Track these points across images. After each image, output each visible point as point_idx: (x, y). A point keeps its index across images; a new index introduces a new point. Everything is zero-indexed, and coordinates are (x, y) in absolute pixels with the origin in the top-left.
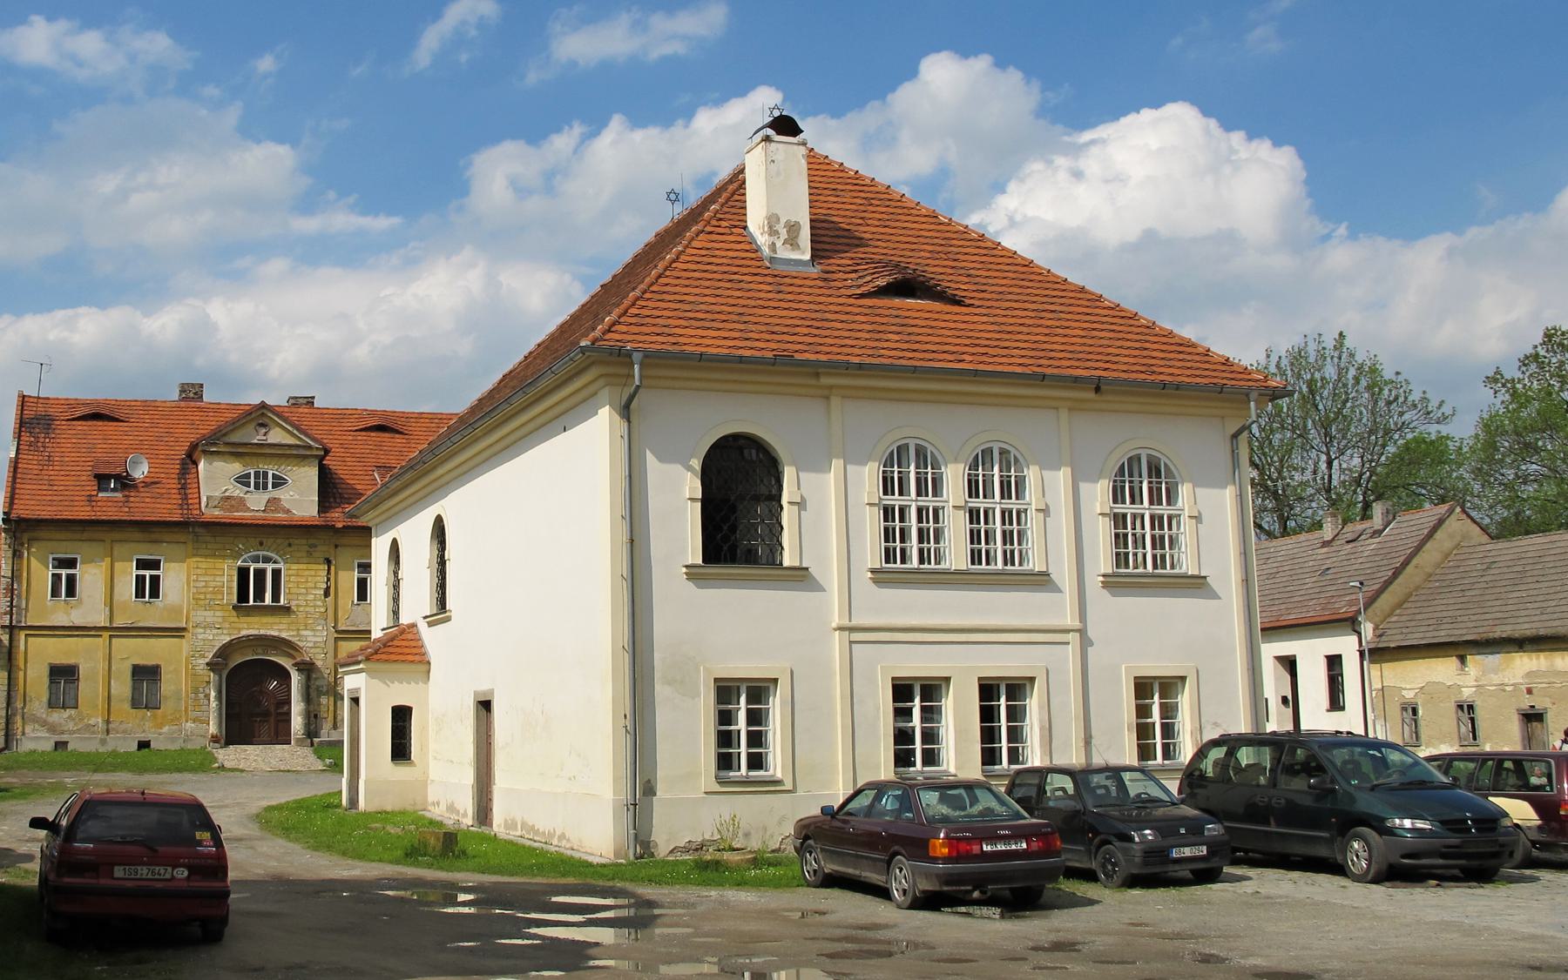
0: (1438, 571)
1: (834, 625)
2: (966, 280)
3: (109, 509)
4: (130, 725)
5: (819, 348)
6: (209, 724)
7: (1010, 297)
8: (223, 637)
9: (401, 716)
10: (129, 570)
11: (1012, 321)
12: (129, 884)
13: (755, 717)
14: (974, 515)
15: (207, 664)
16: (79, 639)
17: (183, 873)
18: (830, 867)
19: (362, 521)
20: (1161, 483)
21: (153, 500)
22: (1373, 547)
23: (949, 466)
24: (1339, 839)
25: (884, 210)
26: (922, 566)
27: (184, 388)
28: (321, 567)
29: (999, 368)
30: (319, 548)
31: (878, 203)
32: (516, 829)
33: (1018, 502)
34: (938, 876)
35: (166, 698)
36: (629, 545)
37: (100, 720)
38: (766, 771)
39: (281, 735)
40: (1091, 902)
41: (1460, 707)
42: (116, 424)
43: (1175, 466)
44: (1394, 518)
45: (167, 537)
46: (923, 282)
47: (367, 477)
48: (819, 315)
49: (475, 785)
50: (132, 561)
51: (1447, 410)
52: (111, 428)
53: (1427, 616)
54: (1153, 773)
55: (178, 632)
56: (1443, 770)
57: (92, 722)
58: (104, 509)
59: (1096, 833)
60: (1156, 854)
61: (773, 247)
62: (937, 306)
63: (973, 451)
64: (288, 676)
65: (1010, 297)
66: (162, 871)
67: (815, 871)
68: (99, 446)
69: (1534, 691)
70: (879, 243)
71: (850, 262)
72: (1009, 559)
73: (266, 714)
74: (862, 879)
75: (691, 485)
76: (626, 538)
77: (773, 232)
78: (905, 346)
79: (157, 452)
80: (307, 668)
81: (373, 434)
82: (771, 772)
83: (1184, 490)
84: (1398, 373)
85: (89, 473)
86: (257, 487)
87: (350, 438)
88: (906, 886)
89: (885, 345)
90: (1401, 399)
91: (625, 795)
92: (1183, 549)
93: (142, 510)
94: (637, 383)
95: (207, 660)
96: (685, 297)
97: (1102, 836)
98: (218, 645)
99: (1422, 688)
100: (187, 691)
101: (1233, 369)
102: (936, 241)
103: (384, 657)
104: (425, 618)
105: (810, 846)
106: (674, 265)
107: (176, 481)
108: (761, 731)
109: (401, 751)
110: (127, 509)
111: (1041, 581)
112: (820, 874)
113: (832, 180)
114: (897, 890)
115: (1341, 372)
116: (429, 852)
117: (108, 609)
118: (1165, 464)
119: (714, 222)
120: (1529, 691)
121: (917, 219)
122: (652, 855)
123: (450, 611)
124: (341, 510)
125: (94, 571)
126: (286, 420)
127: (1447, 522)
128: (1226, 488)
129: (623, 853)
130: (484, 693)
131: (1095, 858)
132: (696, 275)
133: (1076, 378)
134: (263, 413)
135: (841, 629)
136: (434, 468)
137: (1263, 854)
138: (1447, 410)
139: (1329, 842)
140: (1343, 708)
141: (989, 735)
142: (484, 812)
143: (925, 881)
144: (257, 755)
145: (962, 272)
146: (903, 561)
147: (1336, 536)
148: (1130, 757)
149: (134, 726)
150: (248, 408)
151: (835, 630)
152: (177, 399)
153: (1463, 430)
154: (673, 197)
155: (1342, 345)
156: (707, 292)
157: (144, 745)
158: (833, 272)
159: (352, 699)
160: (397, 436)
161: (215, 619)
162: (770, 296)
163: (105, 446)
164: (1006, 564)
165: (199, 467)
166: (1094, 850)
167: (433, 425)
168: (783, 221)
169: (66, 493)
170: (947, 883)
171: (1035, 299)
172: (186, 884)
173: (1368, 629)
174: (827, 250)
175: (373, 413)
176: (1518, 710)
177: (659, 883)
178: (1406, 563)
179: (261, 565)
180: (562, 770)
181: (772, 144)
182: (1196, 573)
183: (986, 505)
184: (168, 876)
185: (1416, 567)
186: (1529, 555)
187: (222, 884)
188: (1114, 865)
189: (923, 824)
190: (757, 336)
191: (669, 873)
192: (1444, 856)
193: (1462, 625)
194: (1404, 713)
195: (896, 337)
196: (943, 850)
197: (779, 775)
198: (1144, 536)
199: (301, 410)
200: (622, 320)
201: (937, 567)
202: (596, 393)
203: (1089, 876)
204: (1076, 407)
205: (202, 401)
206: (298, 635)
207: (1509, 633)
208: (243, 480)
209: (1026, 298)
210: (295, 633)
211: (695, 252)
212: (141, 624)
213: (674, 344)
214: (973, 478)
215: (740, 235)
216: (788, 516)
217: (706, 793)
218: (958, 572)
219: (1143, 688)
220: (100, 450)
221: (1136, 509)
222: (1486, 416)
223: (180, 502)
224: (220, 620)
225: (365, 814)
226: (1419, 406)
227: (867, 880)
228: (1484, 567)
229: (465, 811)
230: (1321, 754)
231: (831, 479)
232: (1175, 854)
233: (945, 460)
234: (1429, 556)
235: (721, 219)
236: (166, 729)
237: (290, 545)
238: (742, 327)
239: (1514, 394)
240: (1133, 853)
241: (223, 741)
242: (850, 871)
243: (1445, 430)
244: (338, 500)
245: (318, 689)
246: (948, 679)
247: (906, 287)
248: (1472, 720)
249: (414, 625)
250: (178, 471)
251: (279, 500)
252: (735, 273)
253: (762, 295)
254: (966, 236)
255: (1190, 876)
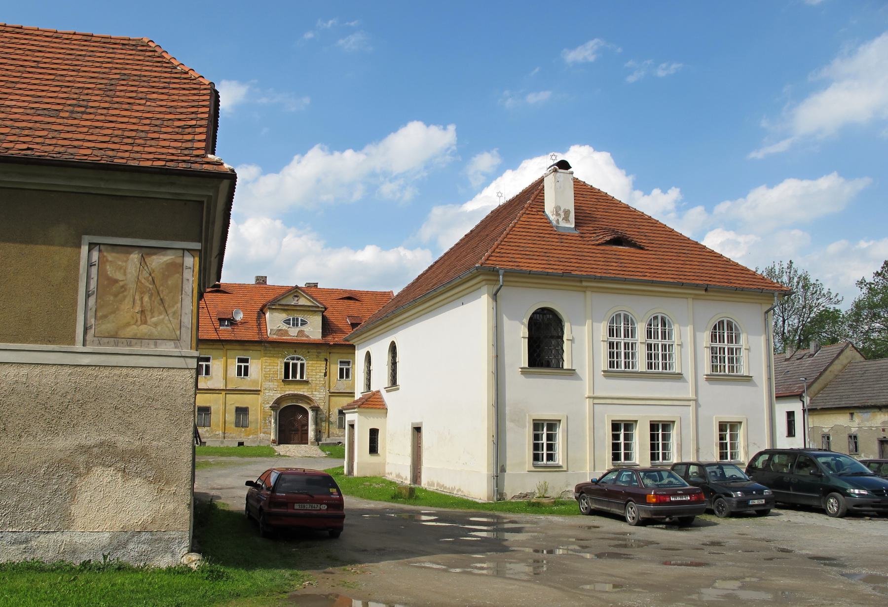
0: (840, 374)
1: (586, 396)
2: (645, 238)
3: (226, 335)
4: (235, 435)
5: (582, 269)
6: (271, 435)
7: (664, 246)
8: (278, 395)
9: (374, 433)
10: (234, 363)
11: (666, 257)
12: (302, 512)
13: (550, 437)
14: (649, 347)
15: (270, 407)
16: (211, 395)
17: (324, 507)
18: (594, 506)
19: (351, 342)
20: (733, 333)
21: (246, 331)
22: (810, 362)
23: (639, 323)
24: (823, 497)
25: (605, 204)
26: (626, 370)
27: (258, 278)
28: (323, 362)
29: (663, 280)
30: (322, 354)
31: (602, 201)
32: (434, 486)
33: (632, 339)
34: (650, 511)
35: (251, 422)
36: (496, 358)
37: (221, 432)
38: (554, 461)
39: (304, 440)
40: (715, 524)
41: (850, 437)
42: (227, 295)
43: (739, 326)
44: (820, 349)
45: (252, 348)
46: (626, 239)
47: (344, 321)
48: (580, 254)
49: (412, 466)
50: (236, 359)
51: (839, 298)
52: (225, 297)
53: (835, 394)
54: (737, 465)
55: (257, 392)
56: (867, 465)
57: (217, 433)
58: (223, 334)
59: (714, 493)
60: (743, 503)
61: (558, 221)
62: (632, 250)
63: (649, 318)
64: (307, 413)
65: (664, 246)
66: (316, 506)
67: (586, 508)
68: (220, 305)
69: (886, 430)
70: (604, 220)
71: (592, 229)
72: (627, 365)
73: (297, 430)
74: (611, 512)
75: (523, 331)
76: (494, 354)
77: (558, 214)
78: (620, 269)
79: (246, 308)
80: (316, 409)
81: (346, 301)
82: (557, 462)
83: (743, 338)
84: (817, 280)
85: (215, 318)
86: (293, 325)
87: (335, 303)
88: (634, 515)
89: (611, 268)
90: (818, 292)
91: (493, 472)
92: (742, 364)
93: (241, 335)
94: (501, 284)
95: (270, 405)
96: (520, 244)
97: (717, 495)
98: (275, 398)
99: (832, 428)
100: (261, 419)
101: (766, 281)
102: (630, 219)
103: (367, 406)
104: (385, 388)
105: (584, 496)
106: (513, 229)
107: (256, 322)
108: (552, 444)
109: (373, 449)
110: (233, 335)
111: (679, 377)
112: (589, 510)
113: (581, 189)
114: (630, 517)
115: (791, 279)
116: (403, 497)
117: (224, 381)
118: (735, 325)
119: (529, 209)
120: (884, 430)
121: (620, 209)
122: (504, 499)
123: (399, 385)
124: (332, 336)
125: (219, 363)
126: (307, 294)
127: (845, 351)
128: (688, 326)
129: (491, 498)
130: (417, 424)
131: (714, 504)
132: (524, 234)
133: (697, 285)
134: (297, 291)
135: (589, 397)
136: (392, 319)
137: (784, 503)
138: (839, 298)
139: (819, 498)
140: (794, 436)
141: (653, 447)
142: (416, 475)
143: (644, 513)
144: (294, 449)
145: (642, 234)
146: (633, 368)
147: (792, 356)
148: (716, 458)
149: (236, 435)
150: (290, 288)
151: (587, 398)
152: (254, 283)
153: (845, 307)
154: (500, 195)
155: (791, 266)
156: (529, 242)
157: (241, 444)
158: (585, 233)
159: (350, 425)
160: (357, 302)
161: (274, 386)
162: (558, 244)
163: (222, 305)
164: (625, 368)
165: (266, 316)
166: (713, 501)
167: (373, 297)
168: (562, 209)
169: (205, 327)
170: (655, 514)
171: (676, 247)
172: (326, 512)
173: (807, 400)
174: (581, 223)
175: (345, 291)
176: (878, 439)
177: (514, 512)
178: (825, 370)
179: (295, 361)
180: (459, 460)
181: (558, 173)
182: (748, 375)
183: (632, 341)
184: (318, 508)
185: (830, 372)
186: (884, 367)
187: (341, 512)
188: (723, 507)
189: (642, 488)
190: (554, 263)
191: (514, 507)
192: (873, 506)
193: (852, 399)
194: (823, 439)
195: (616, 264)
196: (653, 500)
197: (561, 464)
198: (724, 357)
199: (312, 289)
200: (493, 254)
201: (633, 370)
202: (480, 288)
203: (710, 512)
204: (696, 297)
205: (266, 285)
206: (312, 394)
207: (870, 403)
208: (287, 322)
209: (672, 247)
210: (310, 393)
211: (523, 223)
212: (239, 388)
213: (517, 266)
214: (611, 328)
215: (541, 215)
216: (566, 346)
217: (528, 471)
218: (641, 373)
219: (722, 427)
220: (220, 307)
221: (721, 345)
222: (857, 300)
223: (258, 332)
224: (276, 387)
225: (357, 478)
226: (827, 296)
227: (614, 512)
228: (863, 372)
229: (406, 477)
230: (814, 459)
231: (586, 328)
232: (751, 502)
233: (636, 320)
234: (837, 367)
235: (532, 208)
236: (251, 437)
237: (309, 352)
238: (547, 258)
239: (870, 289)
240: (732, 502)
241: (277, 443)
242: (605, 508)
243: (837, 307)
244: (331, 331)
245: (321, 419)
246: (636, 421)
247: (618, 241)
248: (856, 443)
249: (379, 391)
250: (256, 317)
251: (304, 331)
252: (541, 233)
253: (554, 244)
254: (642, 217)
255: (755, 513)
